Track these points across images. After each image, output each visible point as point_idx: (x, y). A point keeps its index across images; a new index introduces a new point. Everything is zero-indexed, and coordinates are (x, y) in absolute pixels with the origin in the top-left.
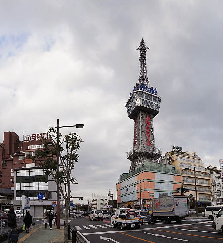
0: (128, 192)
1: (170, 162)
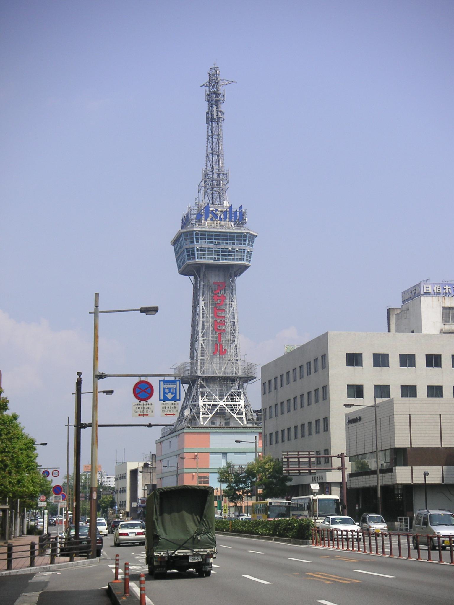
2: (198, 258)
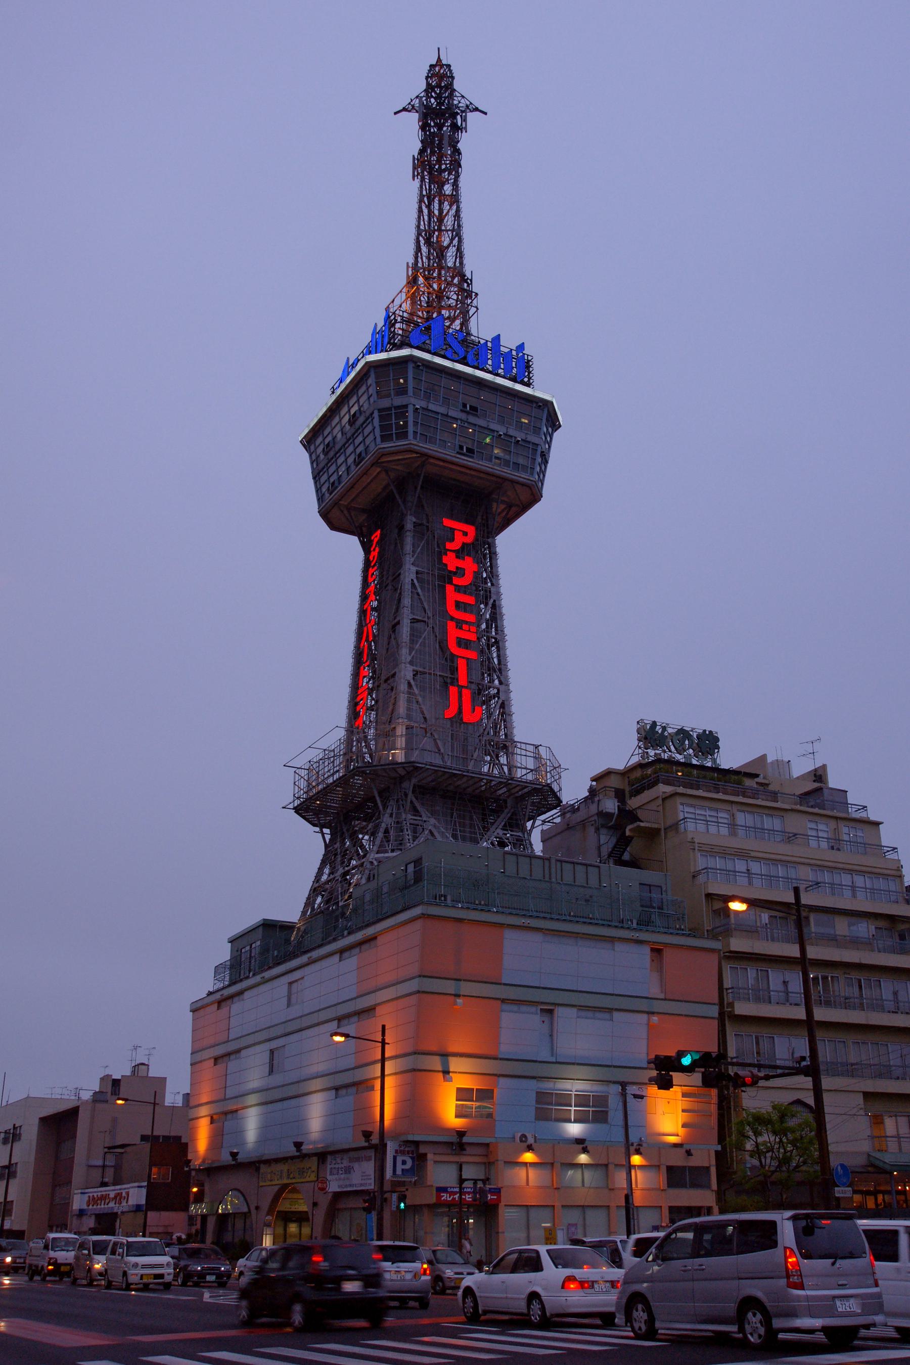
0: (295, 1011)
1: (623, 842)
2: (415, 438)
